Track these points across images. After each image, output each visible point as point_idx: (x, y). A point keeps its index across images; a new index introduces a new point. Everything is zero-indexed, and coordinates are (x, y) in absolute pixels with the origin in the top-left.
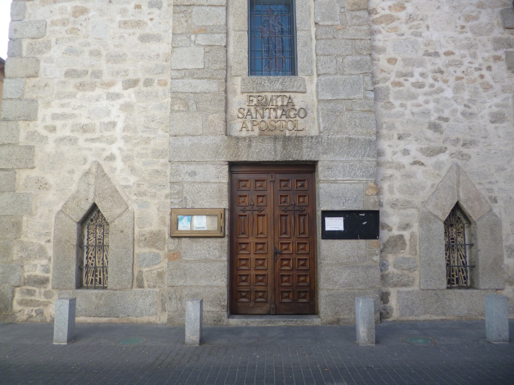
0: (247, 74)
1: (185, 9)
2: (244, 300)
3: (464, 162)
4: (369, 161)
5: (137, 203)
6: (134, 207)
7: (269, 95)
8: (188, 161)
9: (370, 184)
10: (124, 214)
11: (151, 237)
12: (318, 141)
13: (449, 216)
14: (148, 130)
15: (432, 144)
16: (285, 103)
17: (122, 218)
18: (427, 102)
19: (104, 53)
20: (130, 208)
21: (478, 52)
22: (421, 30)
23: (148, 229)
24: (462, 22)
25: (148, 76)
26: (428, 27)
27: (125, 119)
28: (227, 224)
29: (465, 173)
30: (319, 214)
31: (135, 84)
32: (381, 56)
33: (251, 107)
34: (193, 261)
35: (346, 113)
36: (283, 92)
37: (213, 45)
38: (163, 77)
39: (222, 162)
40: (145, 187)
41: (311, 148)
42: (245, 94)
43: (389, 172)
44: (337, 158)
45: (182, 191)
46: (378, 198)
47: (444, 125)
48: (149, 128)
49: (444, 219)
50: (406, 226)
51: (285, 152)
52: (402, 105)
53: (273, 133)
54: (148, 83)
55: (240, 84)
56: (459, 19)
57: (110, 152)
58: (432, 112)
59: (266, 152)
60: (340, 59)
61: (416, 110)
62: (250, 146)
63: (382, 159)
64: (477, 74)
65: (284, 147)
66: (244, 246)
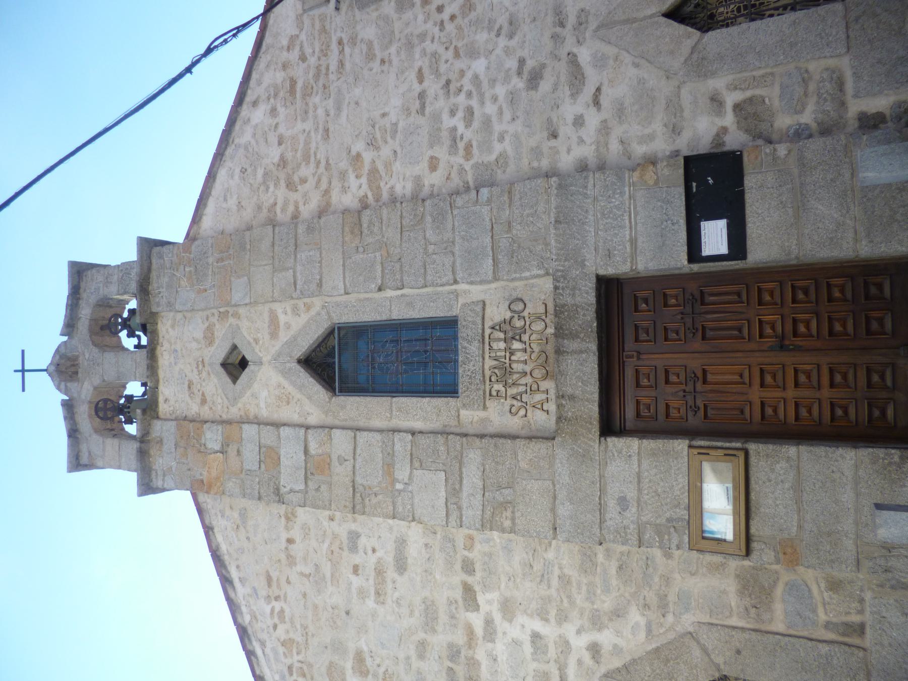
0: (455, 399)
1: (358, 495)
2: (890, 412)
3: (591, 18)
4: (594, 184)
5: (681, 614)
6: (688, 621)
7: (489, 363)
8: (600, 510)
9: (635, 179)
10: (702, 642)
11: (750, 596)
12: (562, 276)
13: (693, 25)
14: (546, 577)
15: (563, 79)
16: (502, 335)
17: (710, 648)
18: (495, 99)
19: (421, 635)
20: (691, 629)
21: (417, 32)
22: (388, 125)
23: (733, 600)
24: (376, 65)
25: (458, 566)
26: (384, 115)
27: (528, 615)
28: (719, 444)
29: (610, 13)
30: (696, 267)
31: (470, 590)
32: (426, 183)
33: (508, 394)
34: (799, 515)
35: (514, 232)
36: (483, 340)
37: (411, 454)
38: (460, 542)
39: (602, 448)
40: (651, 596)
41: (574, 289)
42: (488, 403)
43: (614, 147)
44: (591, 240)
45: (656, 525)
46: (662, 161)
47: (530, 64)
48: (543, 575)
49: (698, 33)
50: (716, 101)
51: (582, 335)
52: (501, 139)
53: (552, 356)
54: (468, 567)
55: (472, 412)
56: (371, 70)
57: (584, 651)
58: (510, 87)
59: (583, 370)
60: (431, 248)
61: (507, 115)
62: (572, 398)
63: (592, 162)
64: (450, 27)
65: (574, 336)
66: (769, 411)
